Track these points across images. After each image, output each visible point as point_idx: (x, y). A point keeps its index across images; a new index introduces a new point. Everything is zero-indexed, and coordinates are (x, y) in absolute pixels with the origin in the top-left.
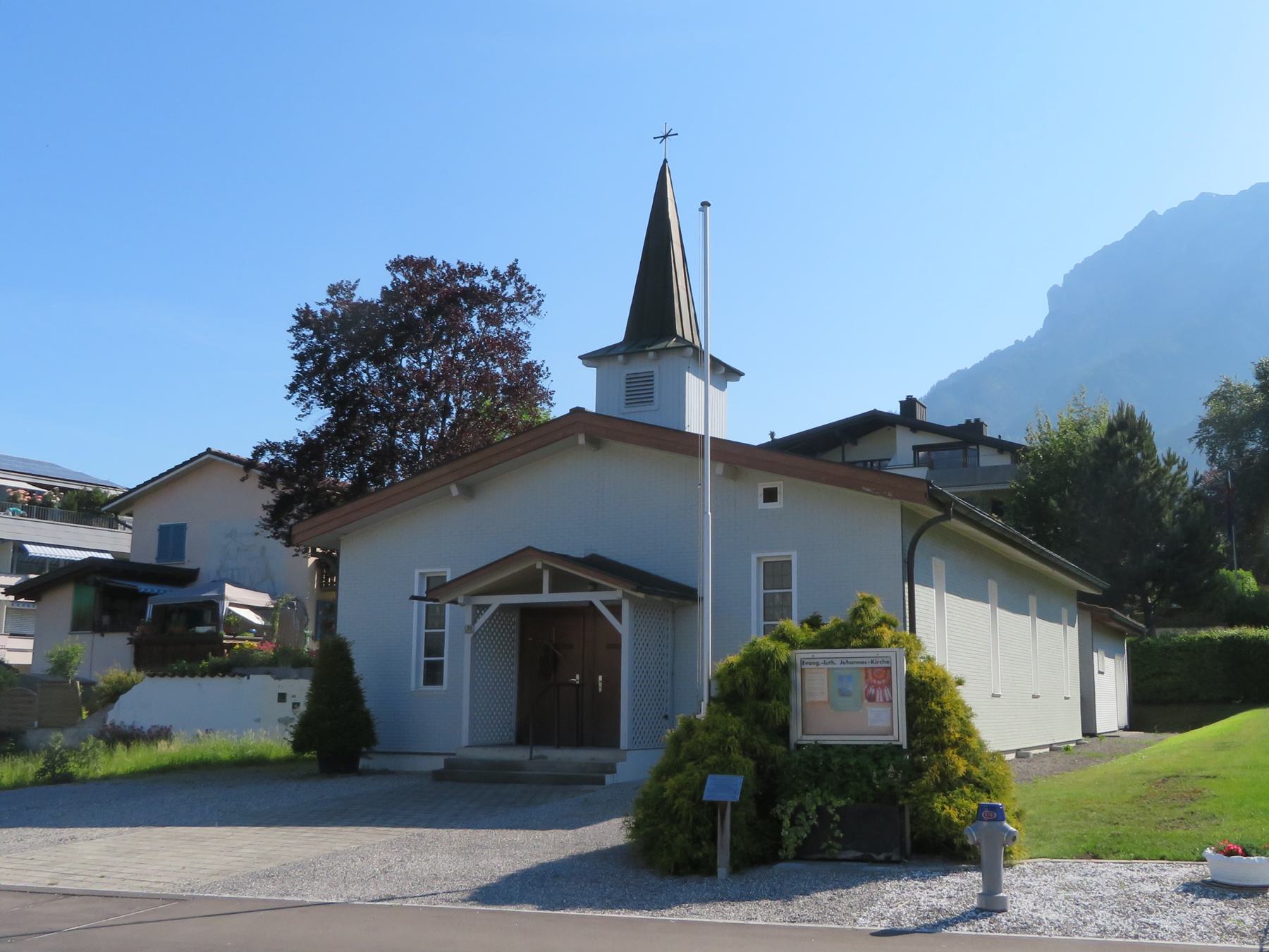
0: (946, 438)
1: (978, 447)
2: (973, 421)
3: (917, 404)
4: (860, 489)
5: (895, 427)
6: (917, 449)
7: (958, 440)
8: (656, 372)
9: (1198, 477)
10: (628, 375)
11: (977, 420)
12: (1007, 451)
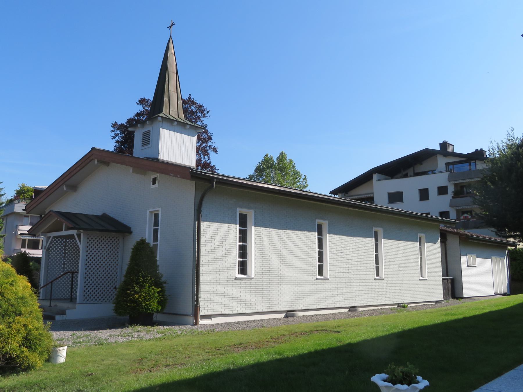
0: (463, 158)
1: (476, 162)
2: (479, 150)
3: (448, 145)
4: (168, 174)
5: (437, 155)
6: (447, 164)
7: (467, 159)
8: (151, 130)
9: (173, 24)
10: (143, 132)
11: (481, 150)
12: (448, 155)
